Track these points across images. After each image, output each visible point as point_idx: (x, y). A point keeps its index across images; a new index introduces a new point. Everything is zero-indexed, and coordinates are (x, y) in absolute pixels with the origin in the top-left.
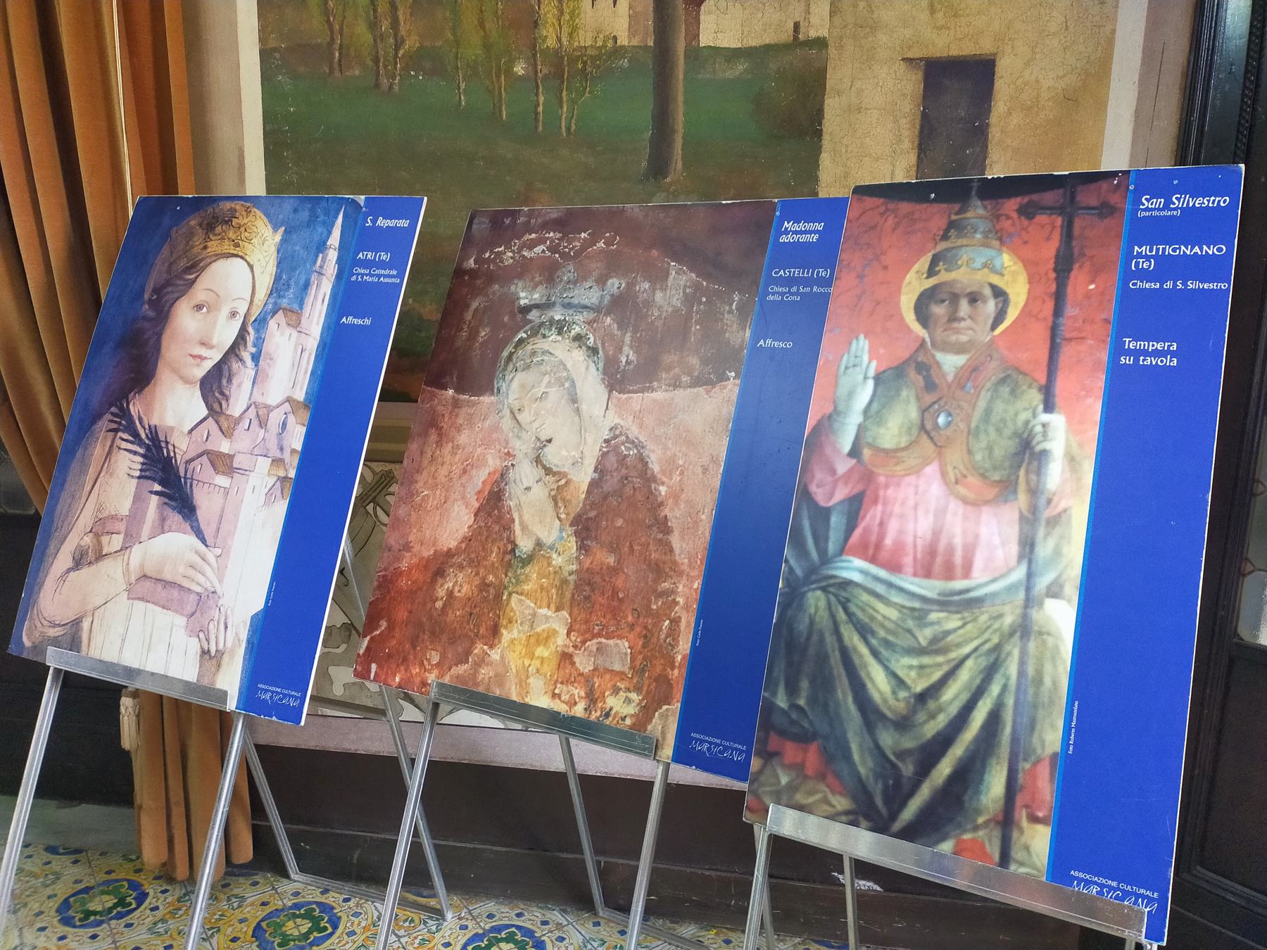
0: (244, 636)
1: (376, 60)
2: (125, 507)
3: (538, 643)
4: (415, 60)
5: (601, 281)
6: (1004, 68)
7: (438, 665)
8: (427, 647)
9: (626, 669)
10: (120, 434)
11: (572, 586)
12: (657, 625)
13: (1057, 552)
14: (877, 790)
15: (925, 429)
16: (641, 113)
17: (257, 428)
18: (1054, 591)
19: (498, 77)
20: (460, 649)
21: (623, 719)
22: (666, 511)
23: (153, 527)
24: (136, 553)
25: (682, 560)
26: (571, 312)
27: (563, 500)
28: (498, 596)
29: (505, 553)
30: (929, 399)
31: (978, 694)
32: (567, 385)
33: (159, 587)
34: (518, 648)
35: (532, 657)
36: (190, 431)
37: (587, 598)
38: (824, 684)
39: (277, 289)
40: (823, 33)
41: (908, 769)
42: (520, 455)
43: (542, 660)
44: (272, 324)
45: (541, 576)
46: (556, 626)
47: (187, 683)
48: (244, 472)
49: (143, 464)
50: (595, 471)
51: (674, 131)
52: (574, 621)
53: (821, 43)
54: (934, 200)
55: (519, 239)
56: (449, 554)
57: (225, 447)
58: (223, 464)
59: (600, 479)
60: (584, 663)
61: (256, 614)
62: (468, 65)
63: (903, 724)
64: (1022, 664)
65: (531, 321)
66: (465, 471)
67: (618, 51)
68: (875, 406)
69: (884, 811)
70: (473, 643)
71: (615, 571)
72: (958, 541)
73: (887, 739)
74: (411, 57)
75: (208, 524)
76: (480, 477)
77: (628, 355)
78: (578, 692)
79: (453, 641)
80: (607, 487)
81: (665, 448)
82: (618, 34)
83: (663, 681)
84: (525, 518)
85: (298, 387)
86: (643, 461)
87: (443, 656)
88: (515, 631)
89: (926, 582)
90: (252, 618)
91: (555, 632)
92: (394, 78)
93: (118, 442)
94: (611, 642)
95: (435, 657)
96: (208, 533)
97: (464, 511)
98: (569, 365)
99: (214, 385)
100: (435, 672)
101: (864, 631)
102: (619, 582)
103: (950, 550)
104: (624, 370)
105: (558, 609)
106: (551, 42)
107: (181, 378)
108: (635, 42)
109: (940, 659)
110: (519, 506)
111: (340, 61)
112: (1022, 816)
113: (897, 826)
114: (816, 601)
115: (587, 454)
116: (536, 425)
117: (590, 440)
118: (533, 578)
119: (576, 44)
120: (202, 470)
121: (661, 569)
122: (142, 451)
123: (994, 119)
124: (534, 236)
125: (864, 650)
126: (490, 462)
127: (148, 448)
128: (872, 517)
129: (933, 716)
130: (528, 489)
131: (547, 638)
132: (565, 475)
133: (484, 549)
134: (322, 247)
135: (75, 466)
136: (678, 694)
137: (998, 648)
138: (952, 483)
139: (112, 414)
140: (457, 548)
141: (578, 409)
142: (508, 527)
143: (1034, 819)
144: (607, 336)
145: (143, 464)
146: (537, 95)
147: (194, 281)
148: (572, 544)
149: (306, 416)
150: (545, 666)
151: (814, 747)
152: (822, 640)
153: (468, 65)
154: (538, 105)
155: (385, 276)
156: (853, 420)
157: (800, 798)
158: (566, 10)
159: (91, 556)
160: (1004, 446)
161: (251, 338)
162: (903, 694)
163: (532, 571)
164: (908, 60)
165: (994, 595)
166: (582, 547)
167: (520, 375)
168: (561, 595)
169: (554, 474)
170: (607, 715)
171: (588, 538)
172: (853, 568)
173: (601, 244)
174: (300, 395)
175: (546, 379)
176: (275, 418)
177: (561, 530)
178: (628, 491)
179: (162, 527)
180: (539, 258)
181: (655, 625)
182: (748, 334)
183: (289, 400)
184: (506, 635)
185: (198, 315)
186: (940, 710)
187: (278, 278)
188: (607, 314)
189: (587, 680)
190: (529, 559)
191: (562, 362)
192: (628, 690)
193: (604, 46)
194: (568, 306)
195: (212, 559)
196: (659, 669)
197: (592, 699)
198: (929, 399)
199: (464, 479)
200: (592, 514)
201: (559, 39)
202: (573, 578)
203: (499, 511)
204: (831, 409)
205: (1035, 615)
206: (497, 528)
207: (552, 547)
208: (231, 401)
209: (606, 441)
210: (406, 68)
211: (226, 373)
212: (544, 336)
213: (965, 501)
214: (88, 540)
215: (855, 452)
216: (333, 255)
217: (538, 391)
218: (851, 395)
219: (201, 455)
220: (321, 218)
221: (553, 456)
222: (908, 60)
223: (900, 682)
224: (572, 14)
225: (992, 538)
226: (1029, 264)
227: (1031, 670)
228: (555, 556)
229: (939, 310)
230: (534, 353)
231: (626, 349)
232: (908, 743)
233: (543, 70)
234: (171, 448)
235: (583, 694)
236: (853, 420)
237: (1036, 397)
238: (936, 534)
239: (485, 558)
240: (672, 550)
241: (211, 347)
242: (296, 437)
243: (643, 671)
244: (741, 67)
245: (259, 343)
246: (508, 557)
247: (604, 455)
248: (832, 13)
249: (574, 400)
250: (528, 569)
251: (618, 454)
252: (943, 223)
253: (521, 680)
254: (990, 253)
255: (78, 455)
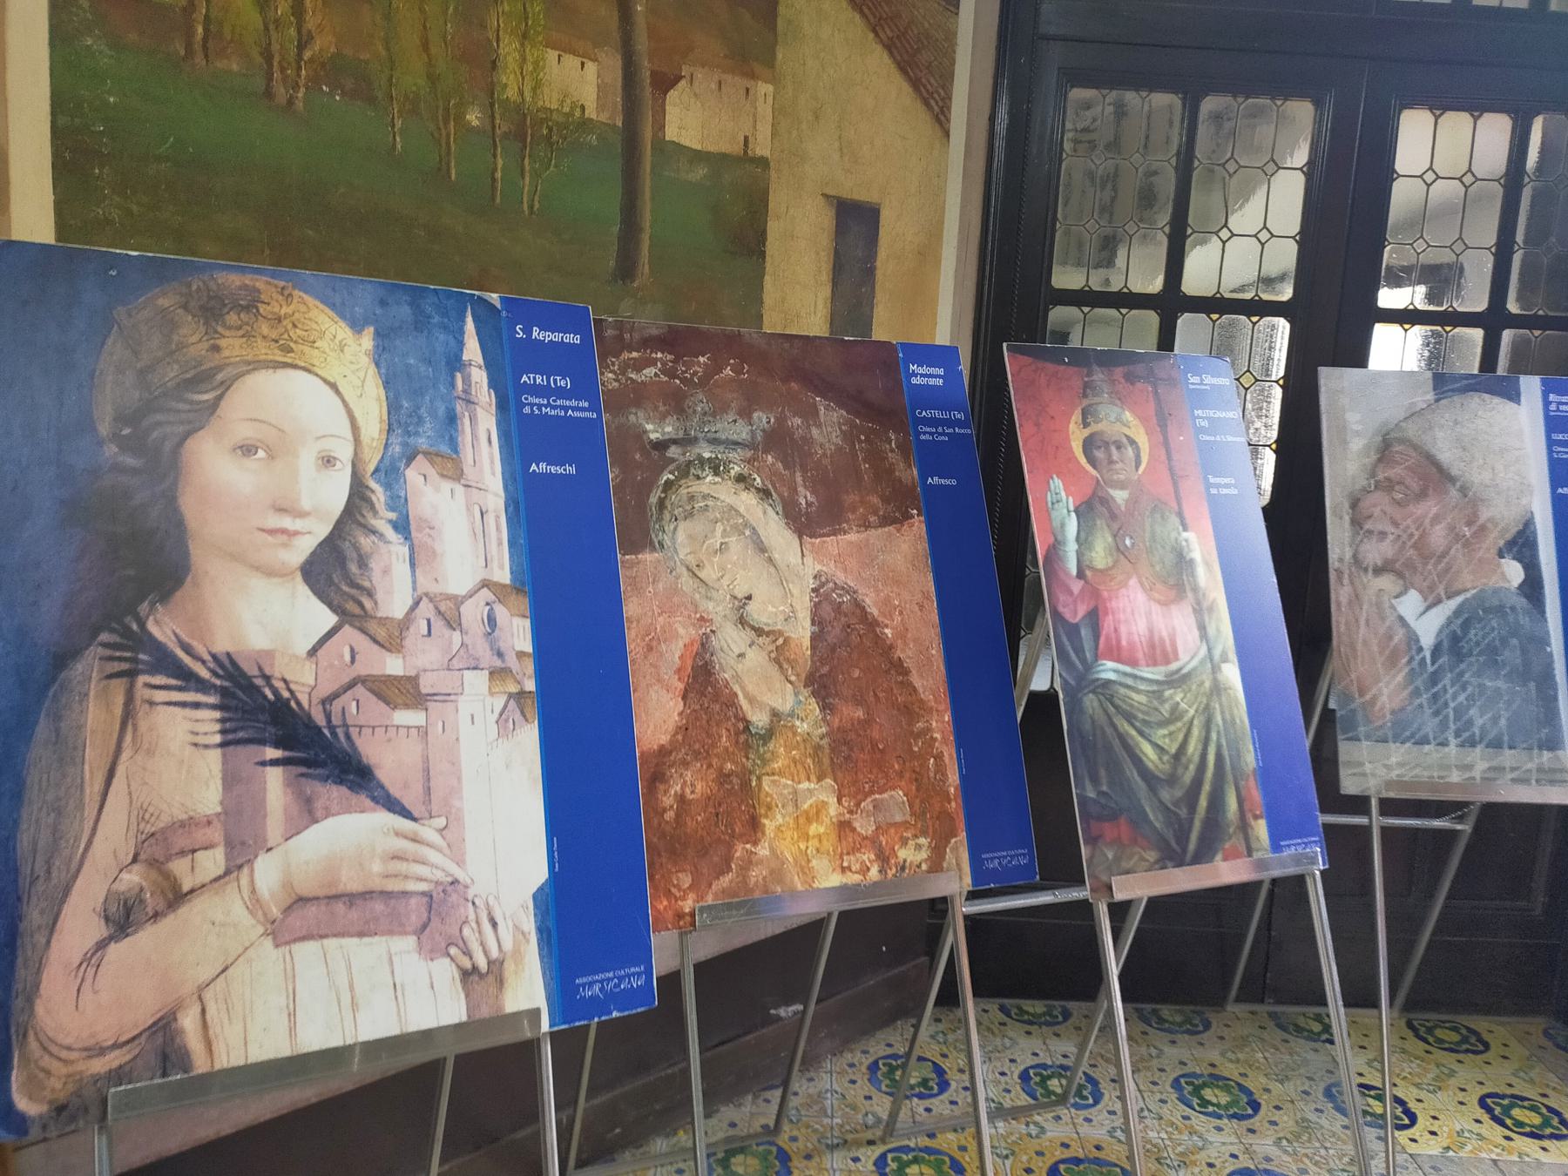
0: (529, 924)
1: (268, 56)
2: (209, 798)
3: (809, 821)
4: (332, 70)
5: (745, 414)
6: (886, 216)
7: (690, 888)
8: (670, 872)
9: (908, 818)
10: (142, 679)
11: (827, 751)
12: (924, 765)
13: (1218, 630)
14: (1170, 836)
15: (1119, 549)
16: (609, 203)
17: (447, 632)
18: (1225, 660)
19: (446, 122)
20: (716, 859)
21: (919, 866)
22: (899, 653)
23: (289, 819)
24: (267, 873)
25: (928, 697)
26: (721, 448)
27: (788, 660)
28: (745, 784)
29: (737, 734)
30: (1115, 526)
31: (1206, 742)
32: (747, 533)
33: (340, 907)
34: (788, 834)
35: (807, 838)
36: (313, 652)
37: (848, 758)
38: (1115, 768)
39: (399, 419)
40: (766, 153)
41: (1183, 813)
42: (718, 619)
43: (819, 837)
44: (412, 475)
45: (788, 748)
46: (823, 797)
47: (458, 1027)
48: (446, 697)
49: (222, 721)
50: (813, 623)
51: (641, 230)
52: (841, 786)
53: (763, 162)
54: (1069, 364)
55: (617, 357)
56: (663, 752)
57: (394, 666)
58: (406, 692)
59: (821, 631)
60: (864, 826)
61: (541, 889)
62: (406, 97)
63: (1172, 780)
64: (1222, 713)
65: (673, 460)
66: (650, 649)
67: (585, 124)
68: (1083, 535)
69: (1178, 849)
70: (730, 847)
71: (867, 722)
72: (1165, 634)
73: (1166, 795)
74: (323, 65)
75: (406, 786)
76: (675, 652)
77: (805, 497)
78: (868, 856)
79: (704, 852)
80: (831, 639)
81: (877, 591)
82: (587, 104)
83: (944, 816)
84: (750, 688)
85: (495, 565)
86: (859, 606)
87: (696, 875)
88: (779, 816)
89: (1155, 669)
90: (535, 897)
91: (824, 804)
92: (296, 87)
93: (141, 692)
94: (885, 796)
95: (686, 880)
96: (409, 800)
97: (665, 697)
98: (742, 510)
99: (334, 571)
100: (691, 896)
101: (1129, 718)
102: (876, 734)
103: (1162, 640)
104: (807, 513)
105: (820, 779)
106: (511, 93)
107: (257, 568)
108: (604, 118)
109: (1179, 724)
110: (737, 677)
111: (205, 40)
112: (1249, 816)
113: (1189, 856)
114: (1090, 702)
115: (798, 607)
116: (725, 582)
117: (795, 592)
118: (780, 753)
119: (540, 103)
120: (360, 709)
121: (911, 710)
122: (212, 699)
123: (878, 264)
124: (635, 354)
125: (1134, 733)
126: (681, 631)
127: (224, 692)
128: (1107, 625)
129: (1187, 768)
130: (742, 655)
131: (818, 813)
132: (780, 633)
133: (709, 736)
134: (455, 362)
135: (39, 753)
136: (961, 824)
137: (1207, 707)
138: (1149, 591)
139: (105, 645)
140: (671, 742)
141: (770, 560)
142: (731, 702)
143: (1256, 817)
144: (773, 475)
145: (222, 721)
146: (495, 156)
147: (214, 405)
148: (813, 706)
149: (524, 604)
150: (825, 842)
151: (1122, 820)
152: (1104, 733)
153: (406, 97)
154: (495, 170)
155: (574, 409)
156: (1071, 548)
157: (1125, 865)
158: (529, 57)
159: (152, 902)
160: (1170, 559)
161: (379, 495)
162: (1166, 758)
163: (778, 746)
164: (825, 195)
165: (1194, 669)
166: (825, 707)
167: (682, 525)
168: (819, 763)
169: (768, 634)
170: (903, 868)
171: (828, 695)
172: (1108, 670)
173: (728, 371)
174: (503, 575)
175: (719, 528)
176: (472, 613)
177: (796, 695)
178: (854, 639)
179: (307, 813)
180: (652, 383)
181: (921, 766)
182: (915, 472)
183: (486, 584)
184: (769, 825)
185: (249, 463)
186: (1189, 761)
187: (393, 407)
188: (766, 451)
189: (873, 841)
190: (769, 734)
191: (732, 508)
192: (916, 836)
193: (571, 114)
194: (714, 442)
195: (435, 837)
196: (937, 807)
197: (883, 858)
198: (1115, 526)
199: (652, 658)
200: (825, 670)
201: (521, 93)
202: (824, 742)
203: (714, 687)
204: (1052, 540)
205: (1220, 677)
206: (717, 707)
207: (792, 714)
208: (380, 596)
209: (813, 590)
210: (315, 81)
211: (351, 553)
212: (698, 478)
213: (1159, 602)
214: (132, 878)
215: (1081, 575)
216: (480, 377)
217: (716, 540)
218: (1063, 525)
219: (351, 685)
220: (436, 319)
221: (760, 612)
222: (825, 195)
223: (1160, 749)
224: (536, 63)
225: (1179, 625)
226: (1144, 420)
227: (1228, 717)
228: (798, 723)
229: (1099, 454)
230: (691, 498)
231: (801, 489)
232: (1179, 793)
233: (503, 126)
234: (279, 685)
235: (873, 857)
236: (1071, 548)
237: (1175, 520)
238: (1151, 631)
239: (714, 745)
240: (915, 690)
241: (302, 514)
242: (519, 634)
243: (924, 813)
244: (700, 173)
245: (399, 503)
246: (742, 738)
247: (817, 605)
248: (773, 135)
249: (762, 548)
250: (771, 746)
251: (832, 602)
252: (1080, 384)
253: (802, 868)
254: (1116, 409)
255: (42, 730)
